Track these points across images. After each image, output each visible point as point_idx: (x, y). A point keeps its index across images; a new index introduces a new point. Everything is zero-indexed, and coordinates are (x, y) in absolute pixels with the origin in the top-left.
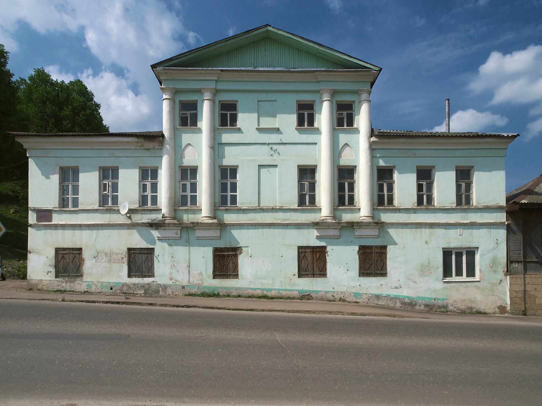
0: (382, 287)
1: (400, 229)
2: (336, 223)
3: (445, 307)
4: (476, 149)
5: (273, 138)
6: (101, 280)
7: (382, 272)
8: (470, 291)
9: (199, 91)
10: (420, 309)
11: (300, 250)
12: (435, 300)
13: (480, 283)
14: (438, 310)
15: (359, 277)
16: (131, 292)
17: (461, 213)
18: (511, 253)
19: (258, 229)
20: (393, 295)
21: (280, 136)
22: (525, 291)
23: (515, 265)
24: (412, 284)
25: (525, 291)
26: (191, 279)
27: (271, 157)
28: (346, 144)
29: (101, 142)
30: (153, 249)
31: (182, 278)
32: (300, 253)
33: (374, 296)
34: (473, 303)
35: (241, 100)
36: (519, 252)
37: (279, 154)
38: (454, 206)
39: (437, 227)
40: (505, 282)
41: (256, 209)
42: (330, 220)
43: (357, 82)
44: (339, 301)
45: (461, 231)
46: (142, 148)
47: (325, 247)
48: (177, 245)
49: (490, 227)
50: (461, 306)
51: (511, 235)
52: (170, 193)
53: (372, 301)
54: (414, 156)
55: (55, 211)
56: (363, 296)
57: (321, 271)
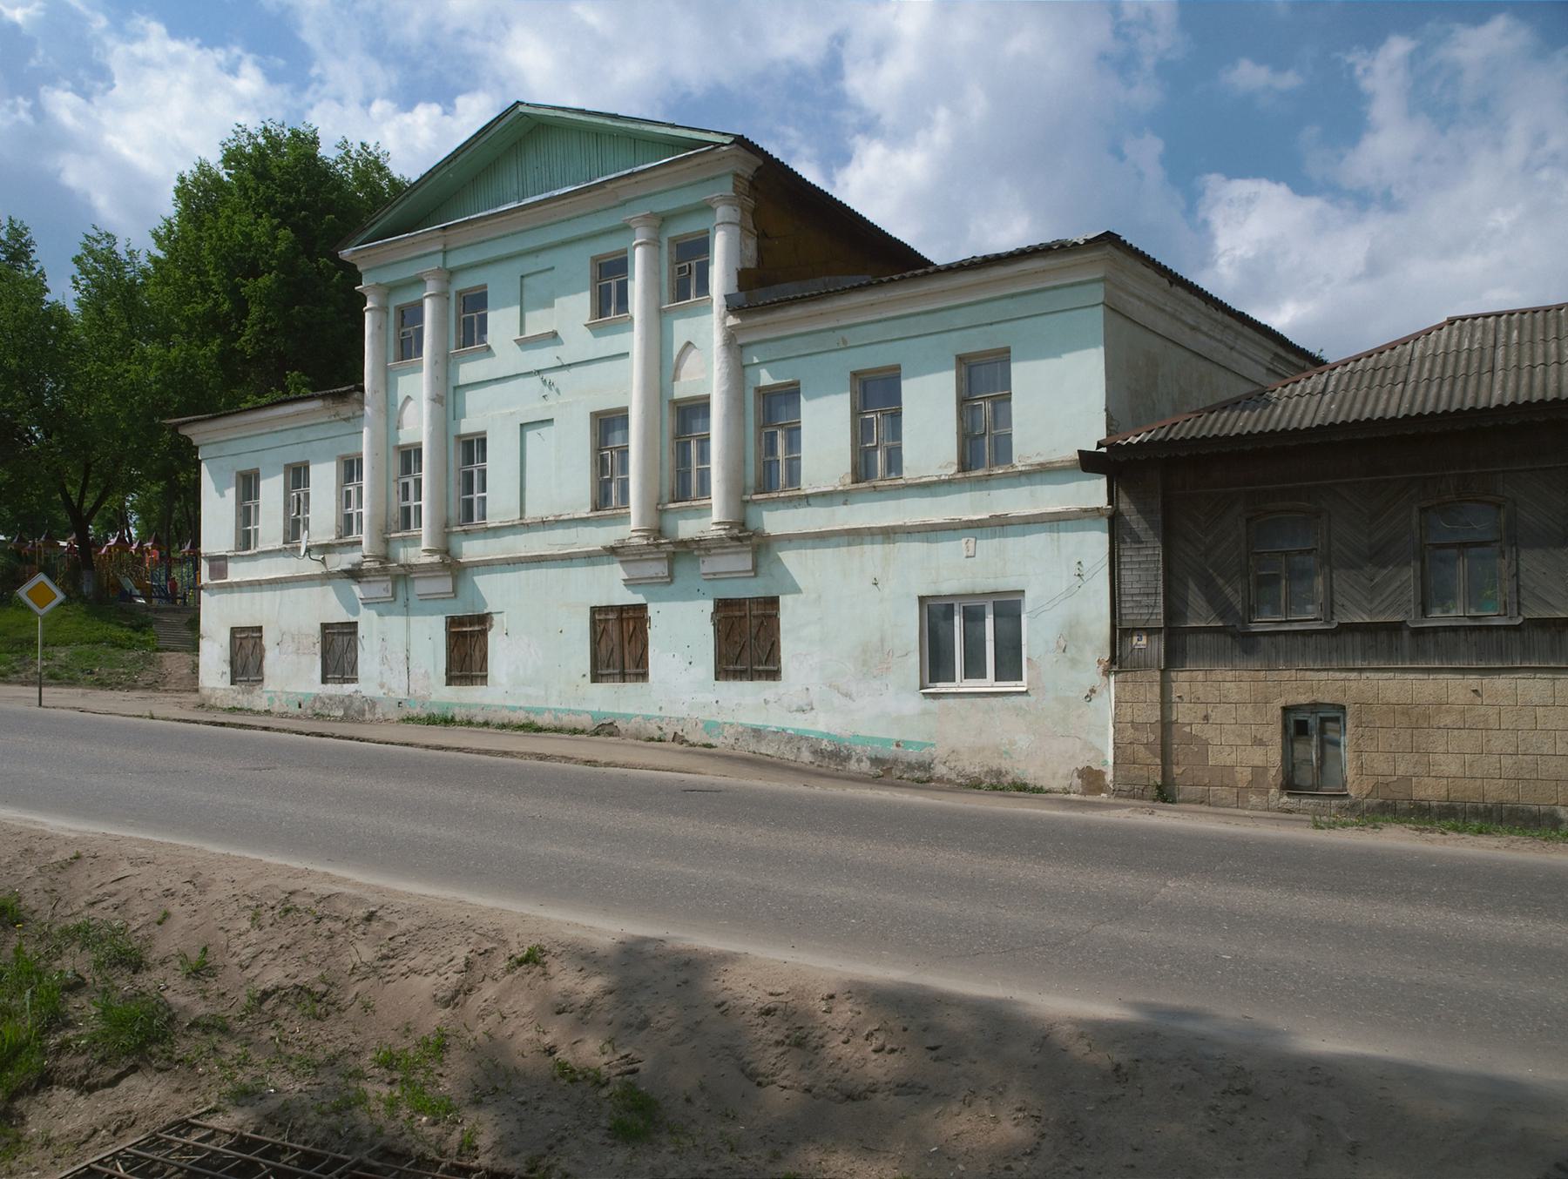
0: (768, 706)
2: (648, 545)
3: (926, 766)
4: (1013, 296)
5: (544, 357)
7: (772, 668)
8: (998, 723)
9: (419, 282)
11: (597, 617)
12: (898, 745)
14: (905, 776)
15: (716, 679)
16: (326, 712)
17: (971, 491)
19: (520, 570)
20: (793, 729)
22: (1166, 725)
25: (1166, 725)
27: (544, 403)
28: (408, 398)
29: (281, 417)
30: (355, 624)
35: (496, 281)
36: (1151, 600)
37: (558, 391)
38: (585, 511)
40: (1106, 695)
41: (513, 526)
42: (637, 540)
45: (971, 545)
46: (337, 418)
47: (642, 608)
48: (390, 613)
54: (843, 346)
56: (723, 730)
57: (637, 667)
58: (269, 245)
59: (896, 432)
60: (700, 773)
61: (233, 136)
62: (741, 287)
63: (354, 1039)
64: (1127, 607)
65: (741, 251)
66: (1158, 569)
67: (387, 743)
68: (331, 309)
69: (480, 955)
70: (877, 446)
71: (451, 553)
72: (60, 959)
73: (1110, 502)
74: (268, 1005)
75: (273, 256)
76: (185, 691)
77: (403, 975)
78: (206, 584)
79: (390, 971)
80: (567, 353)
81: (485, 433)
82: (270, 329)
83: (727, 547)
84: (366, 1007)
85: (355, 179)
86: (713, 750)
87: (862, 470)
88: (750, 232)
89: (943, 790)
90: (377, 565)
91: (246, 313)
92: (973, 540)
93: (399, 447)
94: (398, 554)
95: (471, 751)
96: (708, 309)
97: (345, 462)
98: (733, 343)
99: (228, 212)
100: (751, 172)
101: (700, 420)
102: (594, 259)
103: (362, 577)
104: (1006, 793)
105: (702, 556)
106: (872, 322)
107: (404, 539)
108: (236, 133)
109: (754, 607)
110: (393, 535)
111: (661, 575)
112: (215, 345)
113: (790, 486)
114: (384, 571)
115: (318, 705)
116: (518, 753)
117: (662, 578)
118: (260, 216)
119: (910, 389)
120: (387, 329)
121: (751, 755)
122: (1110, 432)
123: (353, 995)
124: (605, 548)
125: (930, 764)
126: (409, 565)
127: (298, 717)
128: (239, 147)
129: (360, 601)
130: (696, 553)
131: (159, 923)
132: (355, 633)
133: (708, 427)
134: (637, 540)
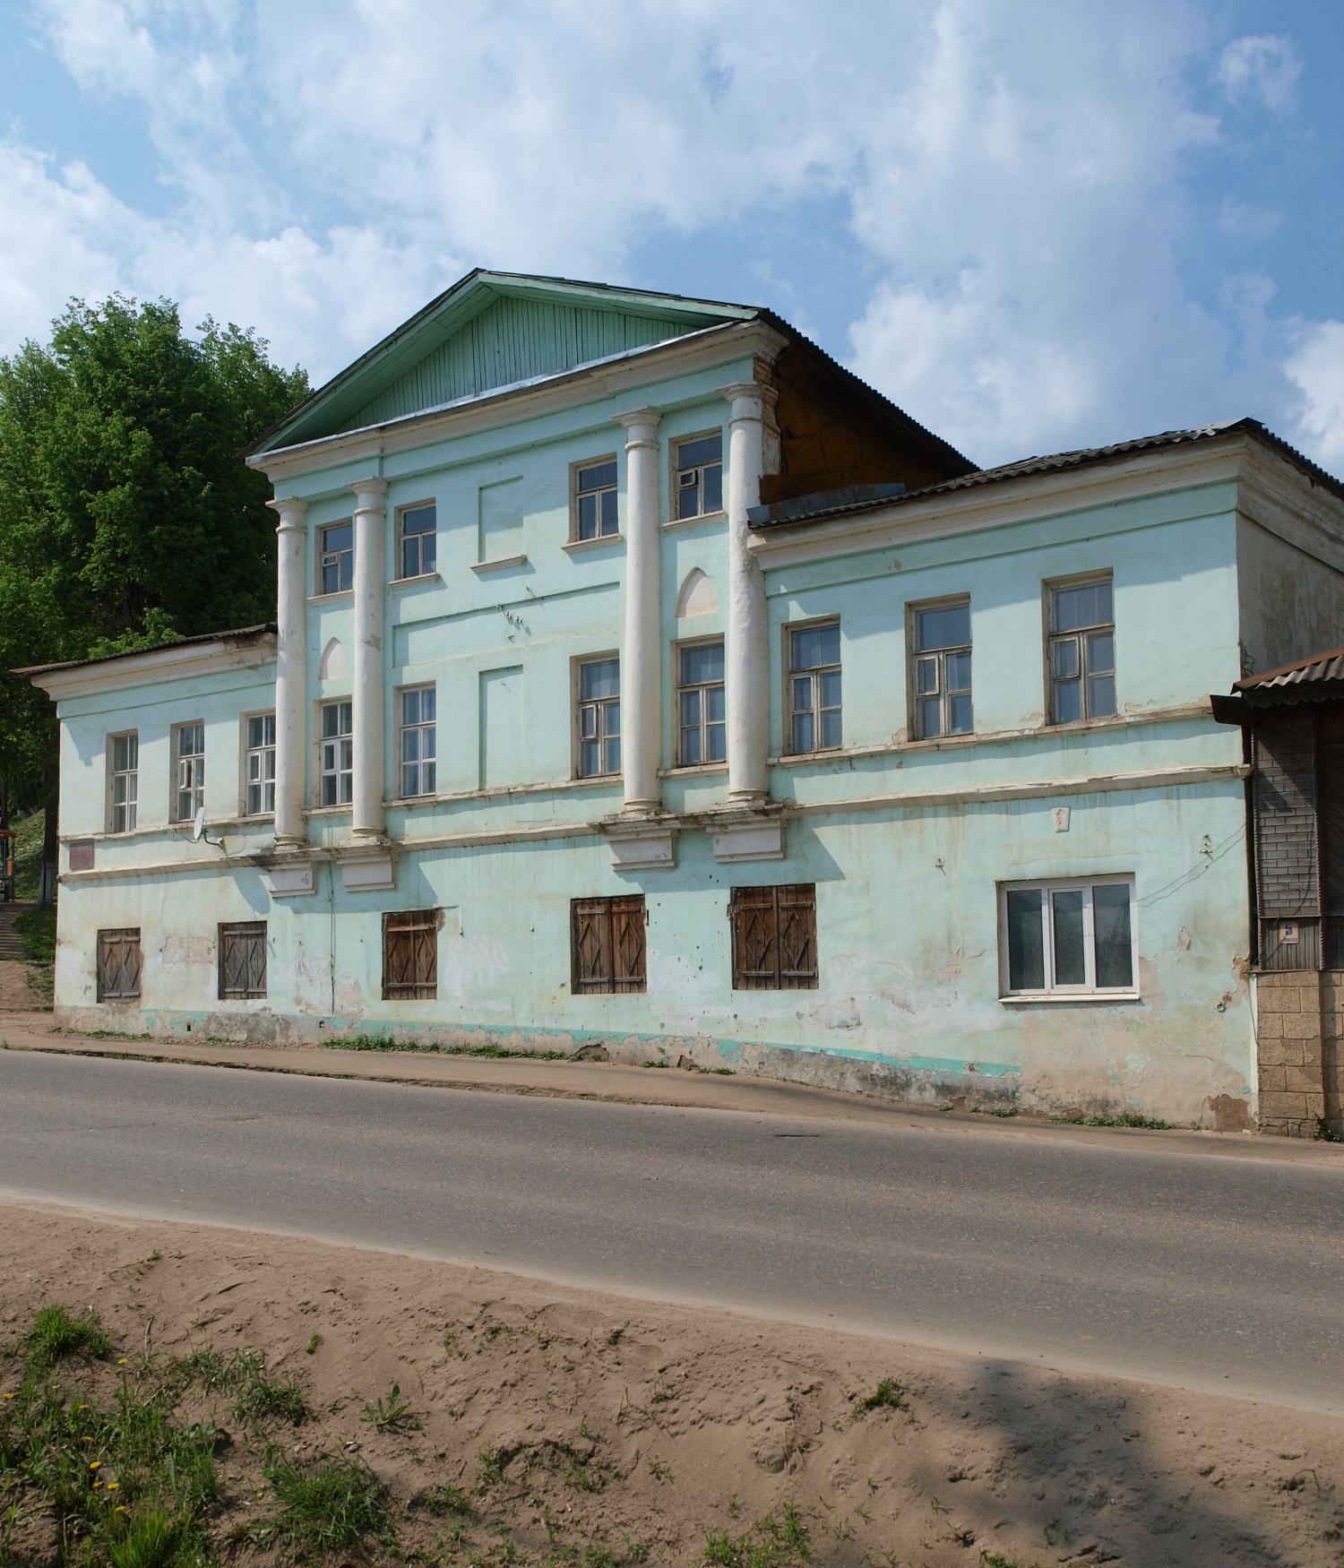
1: (853, 827)
2: (648, 821)
3: (1008, 1095)
4: (1116, 504)
5: (510, 588)
6: (174, 1007)
7: (805, 973)
8: (1103, 1040)
9: (348, 495)
10: (921, 1101)
11: (580, 911)
12: (971, 1069)
13: (1143, 1008)
14: (982, 1108)
17: (1063, 748)
18: (1272, 889)
20: (833, 1050)
21: (529, 580)
23: (1288, 937)
24: (892, 1012)
26: (337, 1001)
28: (334, 641)
29: (166, 665)
30: (262, 925)
31: (319, 1000)
32: (580, 918)
33: (778, 1052)
34: (1113, 1086)
35: (448, 494)
36: (1304, 883)
37: (528, 631)
38: (564, 779)
39: (977, 806)
40: (1245, 1003)
41: (472, 799)
42: (633, 815)
43: (715, 367)
44: (679, 1066)
45: (1064, 816)
46: (242, 666)
47: (639, 899)
48: (310, 910)
49: (1178, 790)
50: (1068, 1092)
51: (1271, 814)
52: (286, 775)
53: (770, 1068)
54: (894, 570)
55: (99, 841)
57: (632, 973)
58: (122, 450)
59: (965, 679)
60: (728, 1108)
61: (67, 312)
62: (764, 499)
63: (659, 1521)
64: (1271, 891)
65: (763, 454)
66: (1311, 843)
67: (320, 1075)
68: (199, 529)
69: (804, 1393)
70: (939, 695)
71: (390, 833)
72: (179, 1405)
73: (1247, 759)
74: (514, 1469)
75: (127, 463)
76: (22, 1010)
77: (694, 1423)
78: (65, 875)
79: (674, 1418)
80: (540, 583)
81: (433, 683)
82: (123, 554)
83: (748, 823)
84: (656, 1472)
85: (222, 367)
86: (731, 1077)
87: (919, 726)
88: (772, 429)
89: (1035, 1126)
90: (295, 850)
91: (92, 534)
92: (1066, 809)
93: (321, 702)
94: (320, 835)
95: (430, 1084)
96: (722, 524)
97: (251, 720)
98: (755, 569)
99: (68, 408)
100: (773, 355)
101: (710, 666)
102: (574, 467)
103: (273, 864)
104: (1117, 1129)
105: (718, 833)
106: (933, 540)
107: (328, 816)
108: (72, 308)
109: (782, 897)
110: (314, 812)
111: (663, 858)
112: (53, 574)
113: (827, 746)
114: (303, 856)
115: (213, 1026)
116: (492, 1085)
117: (664, 862)
118: (108, 413)
119: (983, 624)
120: (306, 556)
121: (781, 1083)
122: (1244, 676)
123: (632, 1454)
124: (592, 826)
125: (1014, 1093)
126: (337, 850)
127: (187, 1043)
128: (74, 327)
129: (270, 896)
130: (709, 830)
131: (311, 1352)
132: (263, 935)
133: (722, 674)
134: (633, 815)
